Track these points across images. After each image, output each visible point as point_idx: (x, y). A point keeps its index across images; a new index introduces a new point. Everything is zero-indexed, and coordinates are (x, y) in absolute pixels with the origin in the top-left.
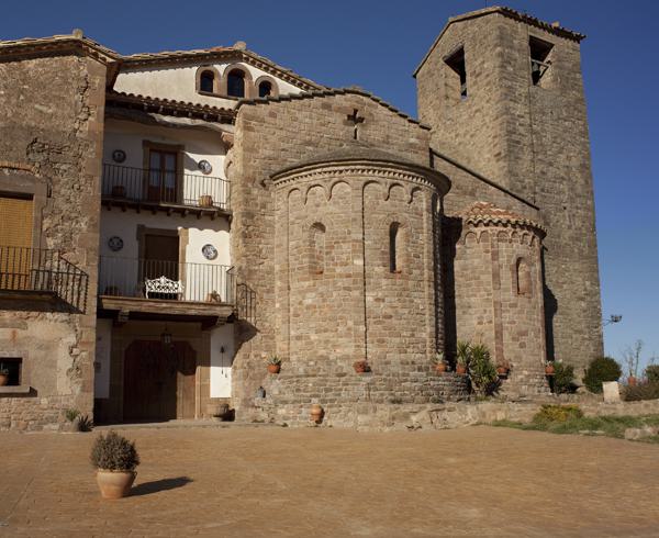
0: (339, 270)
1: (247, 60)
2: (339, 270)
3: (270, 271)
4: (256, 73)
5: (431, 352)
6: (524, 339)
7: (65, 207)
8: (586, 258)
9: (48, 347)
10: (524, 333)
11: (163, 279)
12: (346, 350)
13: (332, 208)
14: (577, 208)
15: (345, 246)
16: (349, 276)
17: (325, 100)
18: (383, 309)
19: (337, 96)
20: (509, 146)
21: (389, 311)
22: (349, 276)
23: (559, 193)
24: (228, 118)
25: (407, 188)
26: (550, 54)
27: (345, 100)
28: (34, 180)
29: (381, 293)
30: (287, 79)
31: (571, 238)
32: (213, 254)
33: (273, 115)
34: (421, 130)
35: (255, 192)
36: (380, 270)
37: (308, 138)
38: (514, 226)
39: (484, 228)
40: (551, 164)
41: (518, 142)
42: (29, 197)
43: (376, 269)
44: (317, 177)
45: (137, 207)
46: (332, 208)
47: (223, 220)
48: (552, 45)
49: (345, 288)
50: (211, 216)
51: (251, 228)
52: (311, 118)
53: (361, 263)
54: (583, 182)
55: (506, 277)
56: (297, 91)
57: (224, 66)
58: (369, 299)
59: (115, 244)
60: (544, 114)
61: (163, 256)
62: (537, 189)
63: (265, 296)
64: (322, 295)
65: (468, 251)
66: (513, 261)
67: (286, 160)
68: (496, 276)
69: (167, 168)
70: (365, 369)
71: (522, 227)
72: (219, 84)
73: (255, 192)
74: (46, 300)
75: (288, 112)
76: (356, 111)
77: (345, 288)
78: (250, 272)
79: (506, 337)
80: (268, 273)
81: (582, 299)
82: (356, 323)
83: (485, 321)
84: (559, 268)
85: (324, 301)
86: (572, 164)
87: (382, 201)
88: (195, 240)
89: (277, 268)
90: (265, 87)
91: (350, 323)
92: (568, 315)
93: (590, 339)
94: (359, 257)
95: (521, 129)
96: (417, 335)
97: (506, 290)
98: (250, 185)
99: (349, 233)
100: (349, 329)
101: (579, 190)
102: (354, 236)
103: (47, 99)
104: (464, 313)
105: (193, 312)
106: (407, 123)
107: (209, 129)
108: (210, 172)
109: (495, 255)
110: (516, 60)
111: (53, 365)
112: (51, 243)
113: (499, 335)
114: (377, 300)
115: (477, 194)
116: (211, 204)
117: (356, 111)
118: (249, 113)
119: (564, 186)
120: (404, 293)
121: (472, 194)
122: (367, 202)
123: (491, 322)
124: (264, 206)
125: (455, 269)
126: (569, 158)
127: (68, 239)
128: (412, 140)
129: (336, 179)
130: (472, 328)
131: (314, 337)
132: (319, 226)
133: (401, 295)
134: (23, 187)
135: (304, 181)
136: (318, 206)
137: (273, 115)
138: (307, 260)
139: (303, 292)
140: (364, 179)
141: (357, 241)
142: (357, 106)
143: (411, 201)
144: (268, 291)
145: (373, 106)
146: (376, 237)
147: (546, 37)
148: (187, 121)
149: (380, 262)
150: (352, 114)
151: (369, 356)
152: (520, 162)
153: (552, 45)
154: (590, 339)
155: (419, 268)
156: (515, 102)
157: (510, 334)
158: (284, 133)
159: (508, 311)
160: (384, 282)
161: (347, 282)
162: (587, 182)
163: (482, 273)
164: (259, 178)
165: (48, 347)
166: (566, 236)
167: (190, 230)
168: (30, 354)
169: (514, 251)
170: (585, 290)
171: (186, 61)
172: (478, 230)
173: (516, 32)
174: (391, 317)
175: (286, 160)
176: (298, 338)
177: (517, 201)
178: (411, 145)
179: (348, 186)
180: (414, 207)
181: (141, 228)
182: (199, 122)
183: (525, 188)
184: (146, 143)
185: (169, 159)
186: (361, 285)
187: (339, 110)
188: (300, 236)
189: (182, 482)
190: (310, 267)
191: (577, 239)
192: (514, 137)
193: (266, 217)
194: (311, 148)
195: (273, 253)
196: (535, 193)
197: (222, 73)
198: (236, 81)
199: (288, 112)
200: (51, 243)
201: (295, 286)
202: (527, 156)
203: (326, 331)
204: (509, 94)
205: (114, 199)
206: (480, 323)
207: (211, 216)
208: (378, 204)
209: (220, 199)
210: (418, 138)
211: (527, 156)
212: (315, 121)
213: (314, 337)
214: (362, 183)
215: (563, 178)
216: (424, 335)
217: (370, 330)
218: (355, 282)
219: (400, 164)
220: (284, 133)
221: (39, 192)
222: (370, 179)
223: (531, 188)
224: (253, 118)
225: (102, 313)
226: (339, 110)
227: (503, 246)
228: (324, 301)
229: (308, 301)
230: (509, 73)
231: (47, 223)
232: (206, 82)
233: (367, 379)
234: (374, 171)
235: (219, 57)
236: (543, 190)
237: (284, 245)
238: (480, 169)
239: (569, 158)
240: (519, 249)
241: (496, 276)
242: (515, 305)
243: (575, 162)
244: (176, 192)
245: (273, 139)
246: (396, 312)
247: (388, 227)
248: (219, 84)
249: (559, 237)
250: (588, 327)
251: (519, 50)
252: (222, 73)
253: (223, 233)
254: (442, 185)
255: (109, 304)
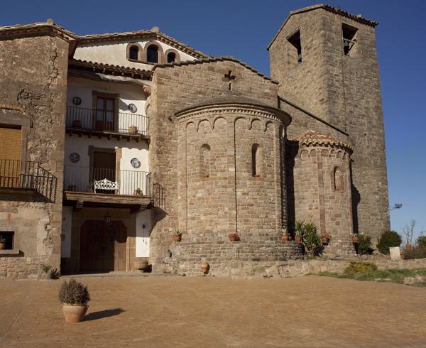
0: (219, 174)
1: (160, 39)
2: (219, 174)
3: (175, 175)
4: (165, 47)
5: (279, 228)
6: (338, 219)
7: (42, 134)
8: (379, 167)
9: (31, 224)
10: (339, 216)
11: (105, 181)
12: (223, 226)
13: (214, 135)
14: (373, 134)
15: (223, 159)
16: (225, 179)
17: (210, 64)
18: (248, 200)
19: (218, 62)
20: (329, 94)
21: (252, 201)
22: (225, 179)
23: (361, 125)
24: (147, 76)
25: (263, 122)
26: (356, 35)
27: (223, 64)
28: (22, 116)
29: (246, 190)
30: (186, 51)
31: (369, 154)
32: (137, 165)
33: (176, 74)
34: (272, 84)
35: (165, 124)
36: (245, 174)
37: (199, 89)
38: (332, 146)
39: (313, 148)
40: (356, 106)
41: (335, 92)
42: (19, 127)
43: (243, 174)
44: (205, 114)
45: (89, 134)
46: (214, 135)
47: (144, 142)
48: (357, 29)
49: (223, 187)
50: (136, 140)
51: (162, 148)
52: (201, 76)
53: (234, 170)
54: (377, 118)
55: (327, 179)
56: (192, 59)
57: (145, 43)
58: (239, 193)
59: (74, 158)
60: (351, 73)
61: (106, 165)
62: (347, 122)
63: (171, 191)
64: (208, 191)
65: (303, 162)
66: (332, 169)
67: (185, 104)
68: (321, 178)
69: (108, 108)
70: (236, 238)
71: (337, 147)
72: (142, 54)
73: (165, 124)
74: (30, 194)
75: (186, 72)
76: (230, 72)
77: (223, 187)
78: (162, 176)
79: (327, 218)
80: (173, 177)
81: (376, 193)
82: (230, 209)
83: (313, 208)
84: (361, 173)
85: (209, 194)
86: (370, 106)
87: (247, 130)
88: (126, 155)
89: (179, 173)
90: (171, 56)
91: (226, 209)
92: (367, 204)
93: (381, 219)
94: (232, 166)
95: (337, 84)
96: (270, 216)
97: (327, 188)
98: (161, 120)
99: (226, 151)
100: (226, 213)
101: (374, 123)
102: (229, 153)
103: (31, 64)
104: (300, 202)
105: (125, 202)
106: (263, 80)
107: (135, 83)
108: (136, 111)
109: (320, 165)
110: (333, 39)
111: (34, 236)
112: (33, 157)
113: (322, 217)
114: (244, 194)
115: (309, 126)
116: (136, 132)
117: (230, 72)
118: (161, 73)
119: (365, 121)
120: (261, 190)
121: (305, 125)
122: (237, 131)
123: (317, 208)
124: (170, 133)
125: (294, 174)
126: (368, 102)
127: (44, 154)
128: (267, 91)
129: (217, 116)
130: (305, 212)
131: (203, 218)
132: (206, 146)
133: (259, 191)
134: (15, 121)
135: (197, 117)
136: (205, 133)
137: (176, 74)
138: (198, 168)
139: (196, 189)
140: (235, 116)
141: (231, 156)
142: (231, 68)
143: (266, 130)
144: (173, 189)
145: (241, 68)
146: (243, 153)
147: (353, 24)
148: (121, 78)
149: (246, 170)
150: (228, 74)
151: (239, 230)
152: (336, 105)
153: (357, 29)
154: (381, 219)
155: (271, 173)
156: (333, 66)
157: (330, 216)
158: (183, 86)
159: (329, 201)
160: (248, 182)
161: (224, 183)
162: (379, 118)
163: (312, 177)
164: (167, 115)
165: (31, 224)
166: (366, 153)
167: (123, 149)
168: (20, 229)
169: (332, 163)
170: (378, 187)
171: (121, 39)
172: (309, 149)
173: (333, 21)
174: (253, 205)
175: (185, 104)
176: (193, 219)
177: (334, 130)
178: (266, 94)
179: (225, 120)
180: (267, 134)
181: (91, 148)
182: (129, 79)
183: (339, 121)
184: (94, 93)
185: (109, 103)
186: (233, 184)
187: (219, 71)
188: (194, 153)
189: (117, 312)
190: (201, 173)
191: (373, 155)
192: (332, 89)
193: (172, 141)
194: (201, 96)
195: (176, 164)
196: (346, 125)
197: (143, 47)
198: (152, 52)
199: (186, 72)
200: (33, 157)
201: (190, 185)
202: (341, 101)
203: (211, 214)
204: (329, 61)
205: (74, 129)
206: (310, 209)
207: (136, 140)
208: (244, 132)
209: (143, 128)
210: (270, 89)
211: (341, 101)
212: (204, 78)
213: (203, 218)
214: (234, 118)
215: (364, 115)
216: (274, 217)
217: (239, 213)
218: (229, 182)
219: (258, 106)
220: (183, 86)
221: (25, 124)
222: (239, 116)
223: (343, 121)
224: (163, 76)
225: (66, 203)
226: (219, 71)
227: (325, 159)
228: (209, 194)
229: (199, 195)
230: (329, 47)
231: (30, 144)
232: (133, 53)
233: (237, 245)
234: (242, 111)
235: (141, 37)
236: (351, 123)
237: (184, 159)
238: (310, 110)
239: (368, 102)
240: (336, 161)
241: (321, 178)
242: (333, 198)
243: (372, 105)
244: (114, 124)
245: (176, 90)
246: (256, 202)
247: (251, 147)
248: (142, 54)
249: (361, 153)
250: (380, 212)
251: (335, 33)
252: (143, 47)
253: (144, 151)
254: (286, 120)
255: (70, 197)
